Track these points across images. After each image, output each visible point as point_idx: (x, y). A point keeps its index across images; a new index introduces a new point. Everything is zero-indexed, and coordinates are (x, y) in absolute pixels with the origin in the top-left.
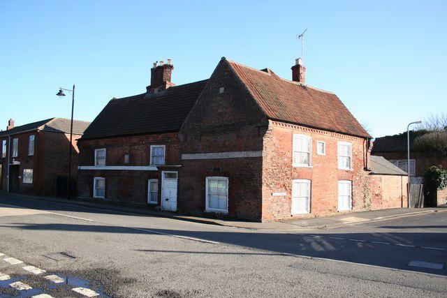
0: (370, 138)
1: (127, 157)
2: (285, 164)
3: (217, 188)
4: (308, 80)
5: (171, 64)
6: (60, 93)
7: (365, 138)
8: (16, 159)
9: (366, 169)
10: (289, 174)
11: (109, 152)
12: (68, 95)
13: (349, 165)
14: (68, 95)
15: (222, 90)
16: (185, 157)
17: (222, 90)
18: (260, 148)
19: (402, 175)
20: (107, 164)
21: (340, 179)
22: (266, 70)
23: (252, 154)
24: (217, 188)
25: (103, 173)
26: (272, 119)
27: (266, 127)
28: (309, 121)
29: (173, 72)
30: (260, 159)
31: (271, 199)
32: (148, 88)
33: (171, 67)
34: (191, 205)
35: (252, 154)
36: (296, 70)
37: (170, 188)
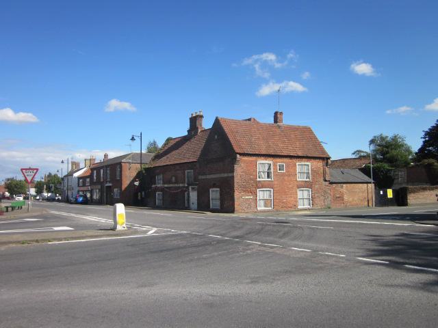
0: (329, 158)
1: (174, 179)
2: (251, 179)
3: (214, 194)
4: (287, 121)
5: (201, 114)
6: (133, 139)
7: (322, 159)
8: (110, 182)
9: (326, 181)
10: (253, 186)
11: (189, 172)
12: (138, 140)
13: (308, 177)
14: (138, 140)
15: (216, 137)
16: (200, 177)
17: (216, 137)
18: (232, 171)
19: (367, 183)
20: (164, 183)
21: (299, 187)
22: (249, 120)
23: (230, 175)
24: (214, 194)
25: (162, 190)
26: (240, 154)
27: (235, 158)
28: (272, 152)
29: (203, 119)
30: (233, 177)
31: (240, 197)
32: (188, 131)
33: (202, 117)
34: (204, 206)
35: (230, 175)
36: (277, 117)
37: (193, 196)
